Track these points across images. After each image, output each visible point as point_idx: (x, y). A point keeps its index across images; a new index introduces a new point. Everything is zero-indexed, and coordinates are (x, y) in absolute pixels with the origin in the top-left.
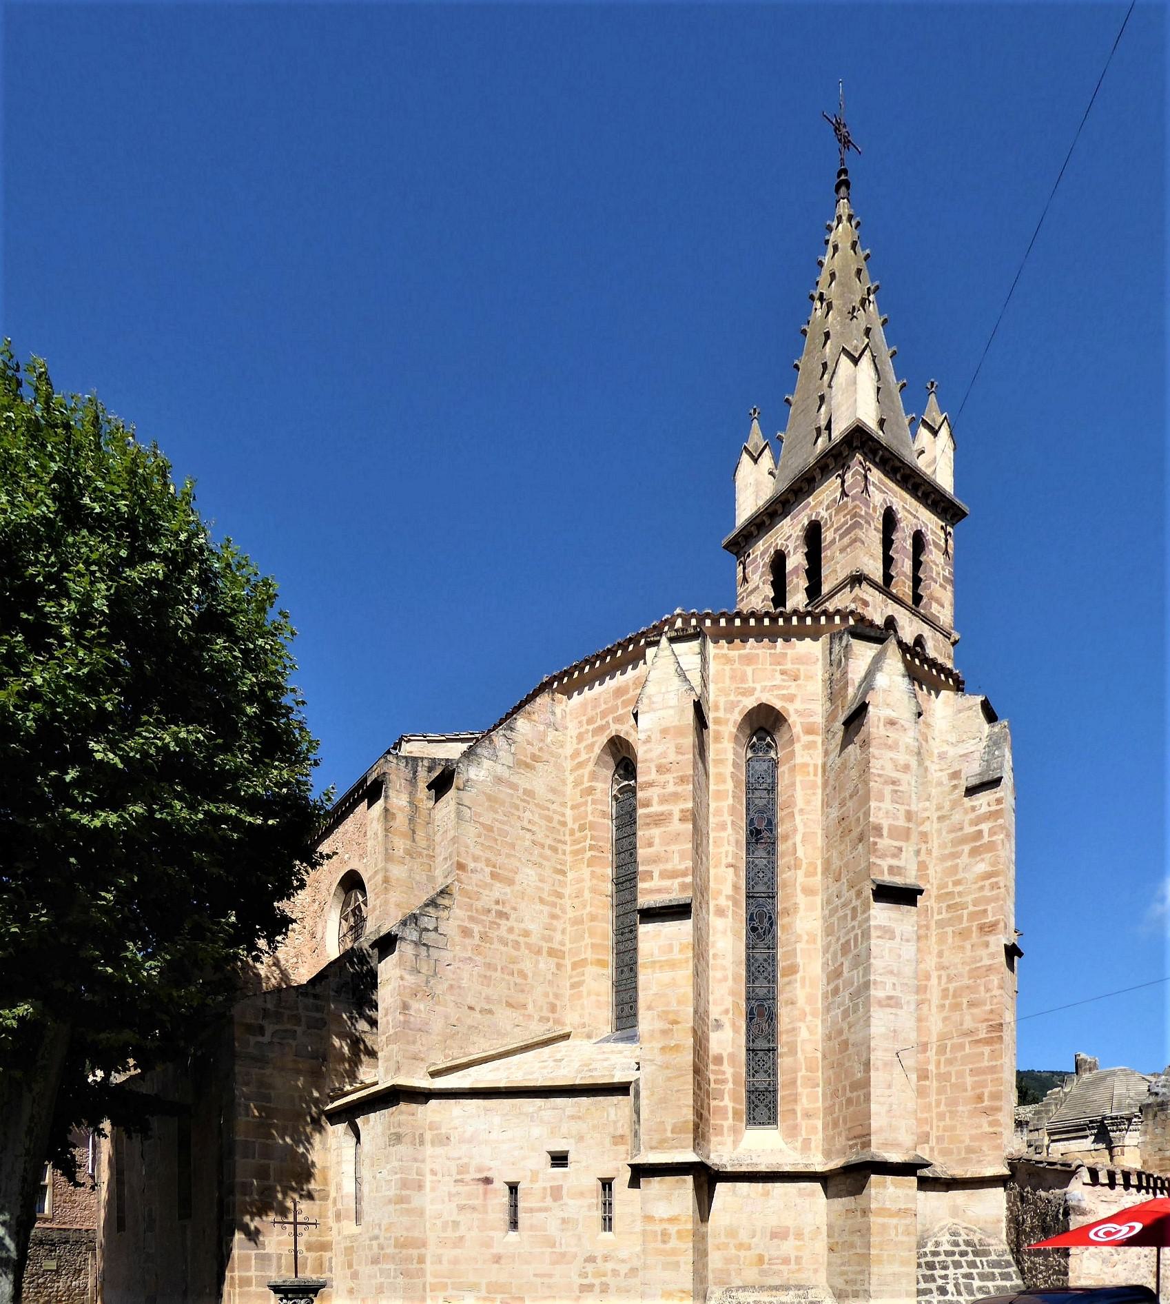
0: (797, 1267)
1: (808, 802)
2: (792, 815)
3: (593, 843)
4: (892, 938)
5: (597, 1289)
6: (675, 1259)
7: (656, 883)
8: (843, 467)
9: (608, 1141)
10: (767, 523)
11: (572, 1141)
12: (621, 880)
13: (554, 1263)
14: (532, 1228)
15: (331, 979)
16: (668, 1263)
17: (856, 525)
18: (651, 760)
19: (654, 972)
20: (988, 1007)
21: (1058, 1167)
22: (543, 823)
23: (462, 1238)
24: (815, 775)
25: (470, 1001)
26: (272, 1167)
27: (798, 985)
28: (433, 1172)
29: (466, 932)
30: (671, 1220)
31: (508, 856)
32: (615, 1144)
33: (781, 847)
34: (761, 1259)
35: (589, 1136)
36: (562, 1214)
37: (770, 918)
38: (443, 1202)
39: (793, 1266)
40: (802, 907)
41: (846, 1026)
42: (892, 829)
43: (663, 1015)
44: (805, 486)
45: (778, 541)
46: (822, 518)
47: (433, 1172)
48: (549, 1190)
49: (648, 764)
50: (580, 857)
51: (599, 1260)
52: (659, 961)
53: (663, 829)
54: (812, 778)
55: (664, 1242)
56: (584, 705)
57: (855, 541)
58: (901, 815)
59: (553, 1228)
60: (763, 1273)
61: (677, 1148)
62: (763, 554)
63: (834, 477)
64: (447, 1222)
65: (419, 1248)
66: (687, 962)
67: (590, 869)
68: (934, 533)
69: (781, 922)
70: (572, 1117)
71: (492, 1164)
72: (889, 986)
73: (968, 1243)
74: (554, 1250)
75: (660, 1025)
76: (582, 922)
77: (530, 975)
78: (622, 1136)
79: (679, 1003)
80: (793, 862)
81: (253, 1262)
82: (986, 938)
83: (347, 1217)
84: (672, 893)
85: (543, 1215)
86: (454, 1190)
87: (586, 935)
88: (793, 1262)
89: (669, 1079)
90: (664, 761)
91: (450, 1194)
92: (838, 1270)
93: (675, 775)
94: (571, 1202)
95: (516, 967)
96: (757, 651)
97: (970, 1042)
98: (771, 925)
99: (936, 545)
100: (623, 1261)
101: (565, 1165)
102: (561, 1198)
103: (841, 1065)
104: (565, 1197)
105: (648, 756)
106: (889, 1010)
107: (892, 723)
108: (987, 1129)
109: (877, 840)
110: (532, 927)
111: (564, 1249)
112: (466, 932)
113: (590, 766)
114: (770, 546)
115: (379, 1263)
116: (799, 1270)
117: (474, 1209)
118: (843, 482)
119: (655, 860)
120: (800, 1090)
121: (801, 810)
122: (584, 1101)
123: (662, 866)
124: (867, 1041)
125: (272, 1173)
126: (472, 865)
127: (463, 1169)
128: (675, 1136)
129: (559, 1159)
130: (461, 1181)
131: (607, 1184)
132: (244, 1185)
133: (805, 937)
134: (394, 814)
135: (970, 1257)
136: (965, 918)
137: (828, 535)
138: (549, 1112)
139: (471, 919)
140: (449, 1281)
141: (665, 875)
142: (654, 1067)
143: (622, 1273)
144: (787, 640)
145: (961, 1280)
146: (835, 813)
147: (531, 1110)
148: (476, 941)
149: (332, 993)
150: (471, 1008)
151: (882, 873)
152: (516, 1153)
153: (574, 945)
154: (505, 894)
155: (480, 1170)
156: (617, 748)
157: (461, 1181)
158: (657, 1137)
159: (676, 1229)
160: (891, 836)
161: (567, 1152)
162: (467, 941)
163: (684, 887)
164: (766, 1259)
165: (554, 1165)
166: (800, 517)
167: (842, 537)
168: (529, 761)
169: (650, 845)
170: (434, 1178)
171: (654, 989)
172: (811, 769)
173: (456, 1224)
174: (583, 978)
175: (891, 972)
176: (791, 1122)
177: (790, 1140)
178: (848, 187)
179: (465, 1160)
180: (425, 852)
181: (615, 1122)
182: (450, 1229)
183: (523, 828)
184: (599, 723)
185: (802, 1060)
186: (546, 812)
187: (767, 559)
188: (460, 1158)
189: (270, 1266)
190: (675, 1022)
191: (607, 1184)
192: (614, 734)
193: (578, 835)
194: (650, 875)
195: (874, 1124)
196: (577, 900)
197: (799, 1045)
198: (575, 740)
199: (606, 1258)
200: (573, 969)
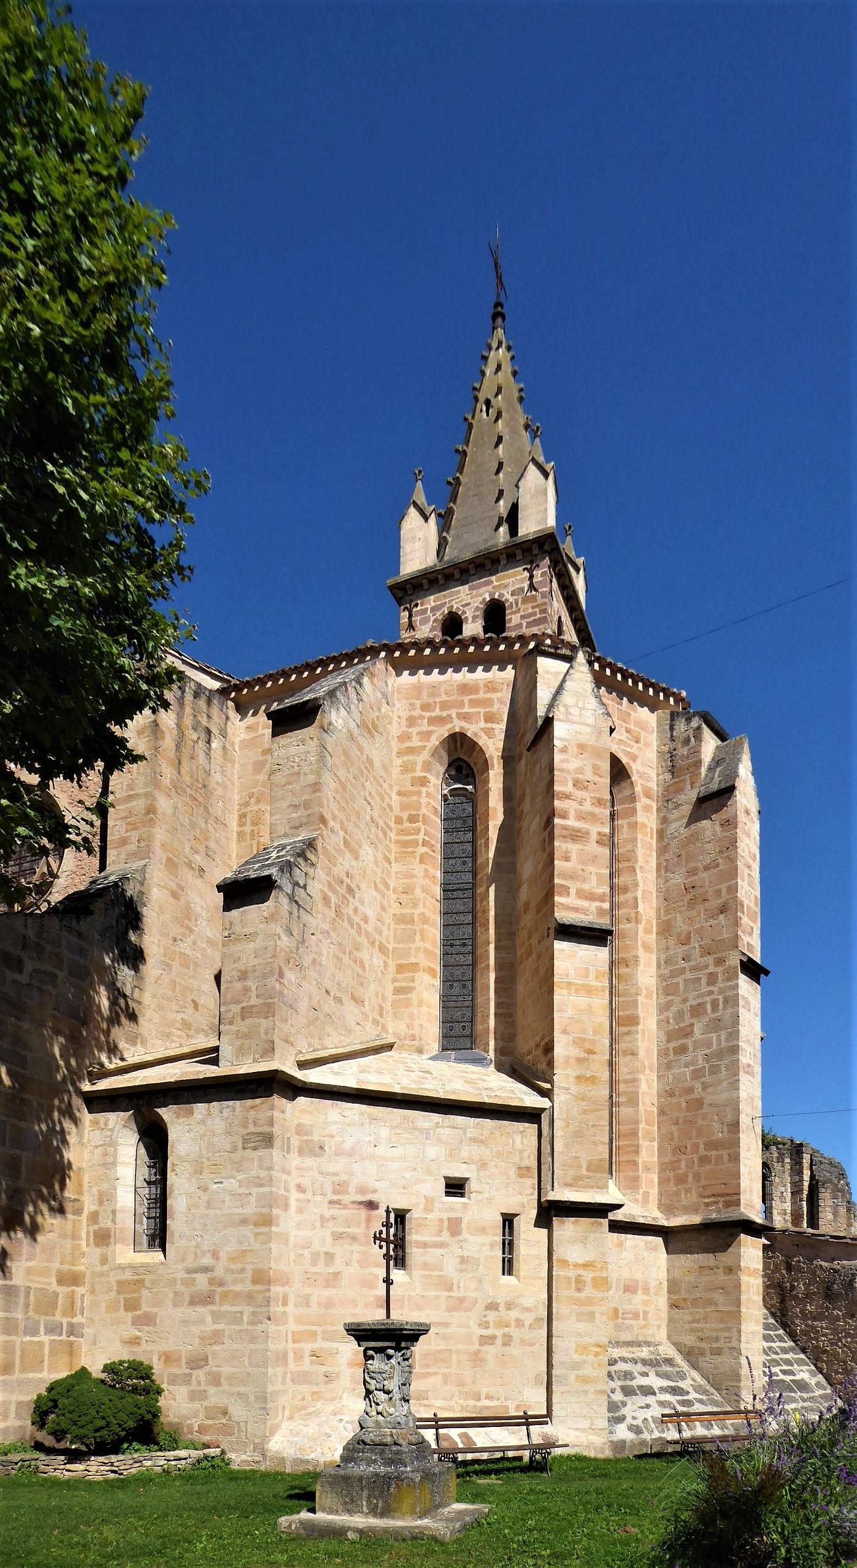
0: (644, 1323)
1: (647, 862)
5: (499, 1341)
6: (590, 1309)
8: (531, 562)
9: (512, 1172)
10: (442, 582)
11: (473, 1167)
12: (450, 887)
13: (450, 1310)
14: (425, 1266)
15: (96, 916)
16: (582, 1313)
18: (568, 772)
19: (569, 994)
21: (849, 1241)
23: (337, 1275)
24: (652, 838)
25: (327, 983)
26: (24, 1160)
27: (639, 1036)
28: (300, 1188)
30: (586, 1266)
32: (521, 1176)
35: (493, 1164)
36: (460, 1252)
38: (314, 1228)
40: (642, 961)
43: (579, 1042)
44: (488, 566)
46: (507, 600)
47: (300, 1188)
48: (446, 1224)
49: (564, 775)
50: (410, 849)
51: (502, 1308)
52: (576, 984)
53: (580, 846)
55: (579, 1290)
56: (418, 688)
59: (450, 1268)
60: (618, 1328)
61: (592, 1187)
62: (433, 609)
63: (521, 569)
64: (318, 1254)
65: (283, 1286)
66: (603, 990)
70: (474, 1140)
71: (378, 1185)
74: (451, 1294)
75: (574, 1052)
76: (411, 921)
78: (528, 1168)
79: (595, 1032)
80: (633, 915)
83: (123, 1241)
84: (588, 914)
85: (439, 1251)
86: (328, 1213)
89: (585, 1112)
90: (581, 776)
91: (323, 1219)
92: (687, 1326)
94: (471, 1238)
95: (358, 954)
100: (528, 1310)
101: (462, 1195)
102: (460, 1233)
103: (690, 1122)
104: (464, 1232)
105: (565, 766)
111: (462, 1294)
113: (425, 755)
114: (443, 605)
115: (212, 1303)
116: (645, 1326)
117: (354, 1239)
118: (531, 577)
119: (572, 877)
120: (641, 1142)
122: (488, 1123)
123: (579, 885)
125: (24, 1170)
126: (331, 823)
127: (340, 1188)
128: (591, 1174)
130: (338, 1202)
131: (508, 1220)
134: (163, 732)
138: (448, 1131)
140: (319, 1329)
141: (582, 894)
142: (568, 1097)
143: (527, 1323)
144: (631, 702)
146: (678, 879)
147: (426, 1125)
149: (97, 936)
152: (408, 1175)
153: (399, 946)
154: (353, 867)
155: (362, 1191)
156: (456, 747)
157: (338, 1202)
158: (572, 1173)
163: (601, 912)
165: (448, 1194)
166: (482, 590)
169: (567, 859)
170: (301, 1196)
171: (570, 1012)
173: (330, 1257)
174: (411, 984)
176: (631, 1173)
177: (629, 1191)
178: (504, 319)
179: (344, 1177)
180: (189, 791)
181: (521, 1152)
182: (321, 1263)
184: (437, 712)
187: (439, 615)
188: (336, 1174)
189: (16, 1303)
190: (590, 1052)
191: (508, 1220)
192: (457, 730)
193: (407, 825)
194: (566, 891)
196: (404, 896)
198: (404, 722)
199: (509, 1306)
200: (398, 972)
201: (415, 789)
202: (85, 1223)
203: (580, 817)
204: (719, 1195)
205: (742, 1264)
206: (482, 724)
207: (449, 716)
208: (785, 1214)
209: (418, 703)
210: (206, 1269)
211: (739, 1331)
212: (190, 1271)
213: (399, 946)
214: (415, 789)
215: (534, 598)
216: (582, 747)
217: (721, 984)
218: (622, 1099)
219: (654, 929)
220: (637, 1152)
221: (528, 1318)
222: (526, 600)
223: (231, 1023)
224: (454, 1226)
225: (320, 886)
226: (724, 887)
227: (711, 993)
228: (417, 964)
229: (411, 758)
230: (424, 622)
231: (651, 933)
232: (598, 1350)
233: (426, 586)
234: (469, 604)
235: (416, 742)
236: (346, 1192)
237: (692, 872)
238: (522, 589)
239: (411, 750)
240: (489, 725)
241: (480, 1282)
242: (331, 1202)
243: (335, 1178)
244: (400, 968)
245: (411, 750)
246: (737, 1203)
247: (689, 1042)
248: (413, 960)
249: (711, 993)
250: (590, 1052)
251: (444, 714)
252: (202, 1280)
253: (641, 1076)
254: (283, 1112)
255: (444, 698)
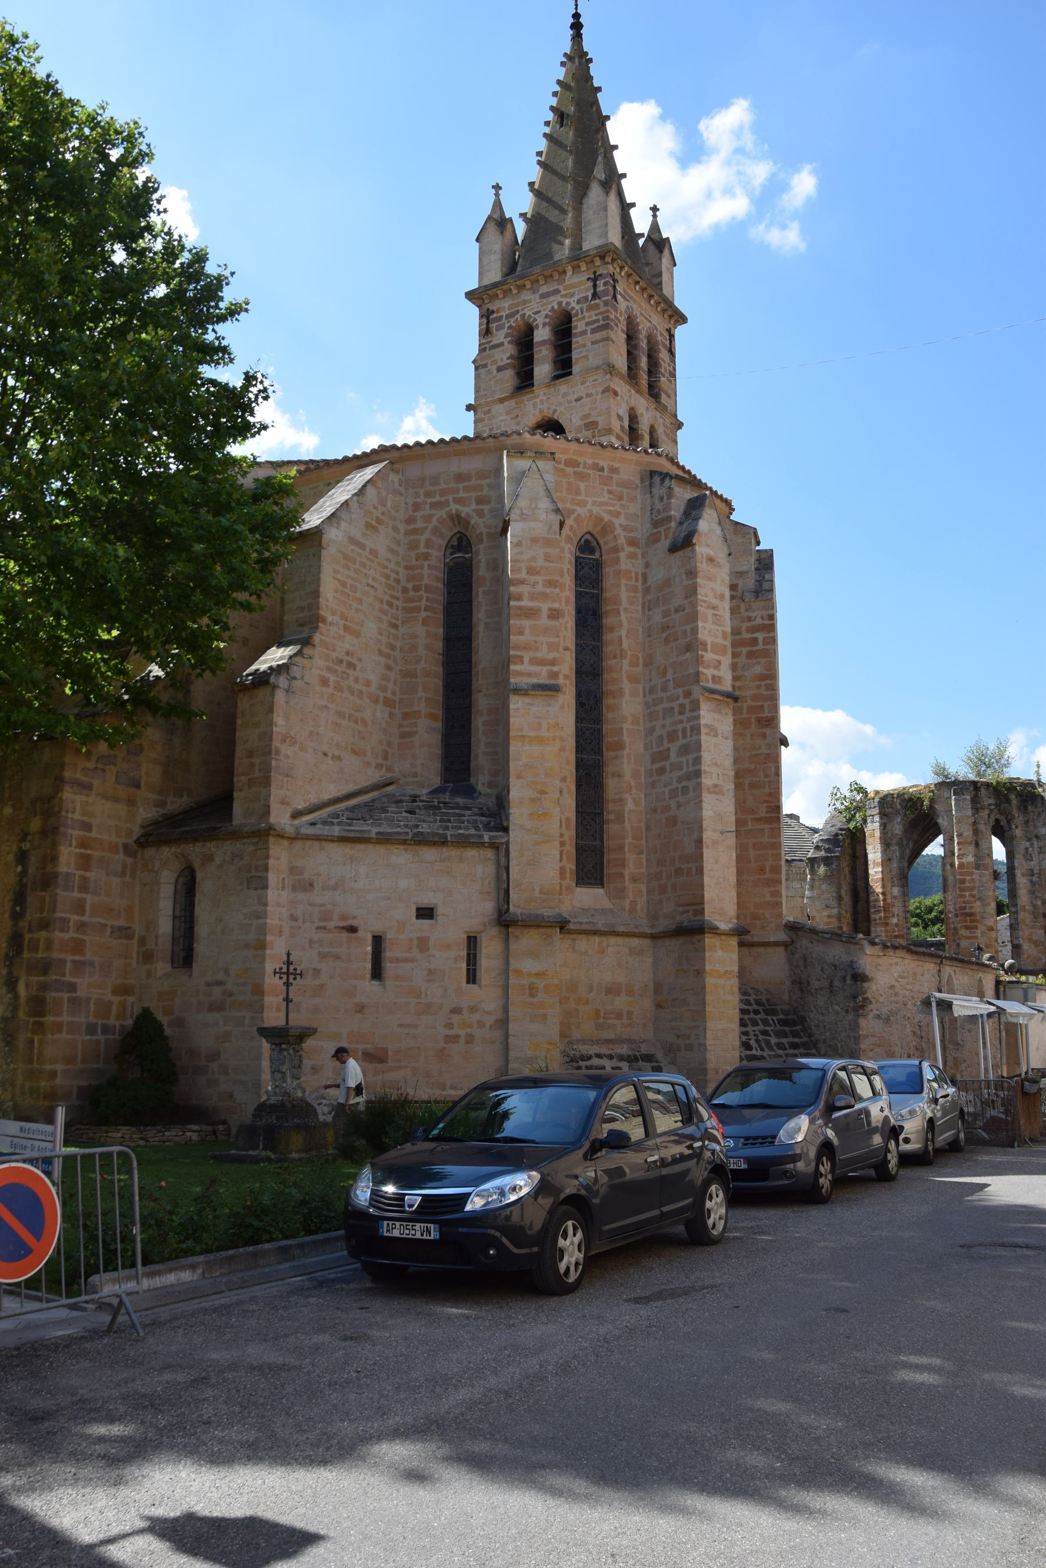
2: (617, 612)
3: (428, 604)
4: (716, 736)
5: (462, 1040)
7: (526, 667)
17: (606, 327)
18: (523, 561)
20: (767, 790)
22: (384, 580)
24: (637, 581)
25: (325, 748)
27: (625, 760)
29: (324, 682)
30: (538, 975)
31: (357, 610)
33: (607, 637)
34: (597, 1013)
37: (595, 696)
39: (625, 1021)
40: (627, 692)
41: (673, 805)
42: (714, 645)
45: (525, 311)
46: (573, 308)
48: (415, 942)
51: (464, 1012)
53: (533, 622)
54: (633, 583)
57: (607, 339)
58: (719, 634)
60: (599, 1027)
67: (425, 628)
68: (662, 334)
69: (608, 701)
72: (714, 776)
73: (758, 1003)
76: (415, 676)
77: (370, 723)
80: (618, 652)
81: (66, 1005)
82: (764, 730)
87: (420, 689)
88: (625, 1016)
90: (534, 564)
93: (544, 578)
96: (589, 471)
97: (752, 819)
98: (596, 702)
99: (664, 345)
102: (428, 950)
106: (715, 796)
107: (711, 560)
108: (768, 898)
109: (704, 653)
110: (372, 677)
112: (324, 682)
116: (630, 1025)
117: (337, 957)
118: (595, 286)
119: (526, 647)
120: (627, 855)
121: (626, 609)
123: (532, 654)
124: (699, 822)
126: (330, 618)
127: (326, 916)
129: (426, 913)
130: (324, 928)
132: (64, 920)
133: (630, 719)
135: (763, 1016)
136: (745, 711)
137: (579, 326)
139: (329, 669)
141: (534, 661)
145: (761, 1037)
148: (331, 690)
150: (325, 754)
151: (708, 681)
153: (406, 696)
155: (343, 918)
159: (543, 983)
160: (713, 652)
161: (436, 905)
162: (325, 689)
164: (602, 1014)
166: (551, 299)
167: (593, 331)
168: (374, 523)
169: (521, 633)
170: (294, 924)
172: (633, 575)
174: (415, 729)
175: (716, 764)
183: (368, 585)
184: (437, 498)
185: (629, 829)
186: (385, 571)
190: (543, 792)
193: (412, 593)
194: (521, 659)
195: (707, 895)
197: (626, 815)
199: (473, 1009)
200: (403, 719)
201: (419, 563)
202: (136, 945)
203: (532, 597)
204: (687, 905)
205: (708, 968)
206: (474, 506)
207: (447, 501)
208: (1032, 875)
209: (422, 491)
210: (220, 983)
211: (705, 1029)
212: (208, 984)
213: (406, 696)
214: (419, 563)
215: (597, 306)
216: (534, 540)
217: (688, 714)
218: (611, 817)
219: (641, 662)
220: (623, 865)
221: (489, 1020)
222: (590, 308)
223: (241, 790)
224: (423, 944)
225: (318, 672)
226: (688, 628)
227: (681, 722)
228: (419, 712)
229: (416, 537)
230: (498, 329)
231: (637, 665)
232: (550, 1047)
233: (501, 296)
234: (539, 312)
235: (420, 524)
236: (331, 920)
237: (666, 614)
238: (586, 298)
239: (415, 531)
240: (480, 507)
241: (446, 990)
242: (318, 928)
243: (322, 909)
244: (405, 716)
245: (415, 531)
246: (702, 912)
247: (667, 764)
248: (416, 709)
249: (681, 722)
250: (543, 792)
251: (443, 499)
252: (217, 991)
253: (626, 796)
254: (278, 859)
255: (443, 486)
